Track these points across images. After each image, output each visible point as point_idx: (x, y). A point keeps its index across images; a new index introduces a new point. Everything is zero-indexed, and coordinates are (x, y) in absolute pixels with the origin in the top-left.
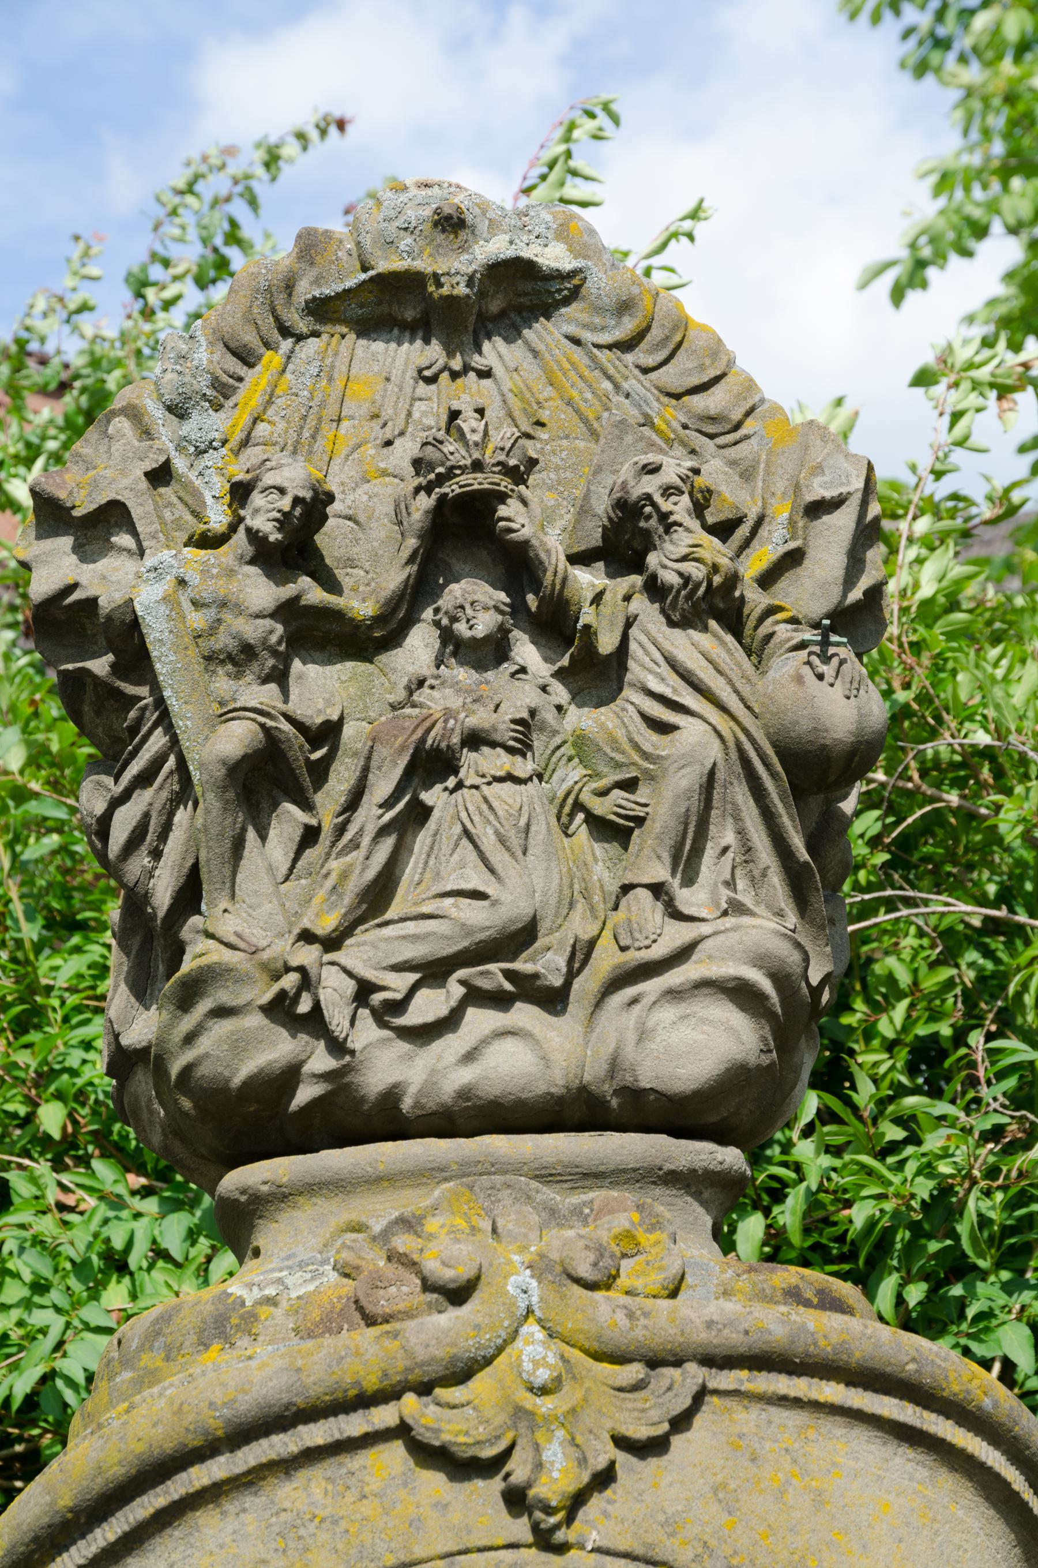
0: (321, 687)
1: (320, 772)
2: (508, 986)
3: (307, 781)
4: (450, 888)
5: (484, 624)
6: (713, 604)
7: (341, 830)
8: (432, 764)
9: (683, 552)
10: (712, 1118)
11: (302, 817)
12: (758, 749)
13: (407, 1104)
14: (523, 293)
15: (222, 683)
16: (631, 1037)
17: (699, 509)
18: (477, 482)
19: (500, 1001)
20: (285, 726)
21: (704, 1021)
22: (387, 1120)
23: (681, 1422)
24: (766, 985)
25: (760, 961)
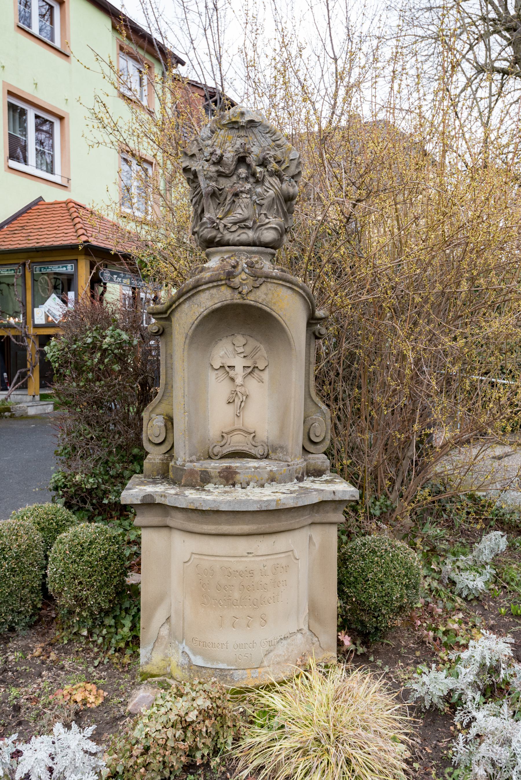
1: (221, 194)
4: (239, 213)
6: (277, 174)
8: (236, 195)
9: (273, 166)
15: (208, 181)
19: (243, 228)
22: (228, 244)
23: (261, 285)
24: (279, 228)
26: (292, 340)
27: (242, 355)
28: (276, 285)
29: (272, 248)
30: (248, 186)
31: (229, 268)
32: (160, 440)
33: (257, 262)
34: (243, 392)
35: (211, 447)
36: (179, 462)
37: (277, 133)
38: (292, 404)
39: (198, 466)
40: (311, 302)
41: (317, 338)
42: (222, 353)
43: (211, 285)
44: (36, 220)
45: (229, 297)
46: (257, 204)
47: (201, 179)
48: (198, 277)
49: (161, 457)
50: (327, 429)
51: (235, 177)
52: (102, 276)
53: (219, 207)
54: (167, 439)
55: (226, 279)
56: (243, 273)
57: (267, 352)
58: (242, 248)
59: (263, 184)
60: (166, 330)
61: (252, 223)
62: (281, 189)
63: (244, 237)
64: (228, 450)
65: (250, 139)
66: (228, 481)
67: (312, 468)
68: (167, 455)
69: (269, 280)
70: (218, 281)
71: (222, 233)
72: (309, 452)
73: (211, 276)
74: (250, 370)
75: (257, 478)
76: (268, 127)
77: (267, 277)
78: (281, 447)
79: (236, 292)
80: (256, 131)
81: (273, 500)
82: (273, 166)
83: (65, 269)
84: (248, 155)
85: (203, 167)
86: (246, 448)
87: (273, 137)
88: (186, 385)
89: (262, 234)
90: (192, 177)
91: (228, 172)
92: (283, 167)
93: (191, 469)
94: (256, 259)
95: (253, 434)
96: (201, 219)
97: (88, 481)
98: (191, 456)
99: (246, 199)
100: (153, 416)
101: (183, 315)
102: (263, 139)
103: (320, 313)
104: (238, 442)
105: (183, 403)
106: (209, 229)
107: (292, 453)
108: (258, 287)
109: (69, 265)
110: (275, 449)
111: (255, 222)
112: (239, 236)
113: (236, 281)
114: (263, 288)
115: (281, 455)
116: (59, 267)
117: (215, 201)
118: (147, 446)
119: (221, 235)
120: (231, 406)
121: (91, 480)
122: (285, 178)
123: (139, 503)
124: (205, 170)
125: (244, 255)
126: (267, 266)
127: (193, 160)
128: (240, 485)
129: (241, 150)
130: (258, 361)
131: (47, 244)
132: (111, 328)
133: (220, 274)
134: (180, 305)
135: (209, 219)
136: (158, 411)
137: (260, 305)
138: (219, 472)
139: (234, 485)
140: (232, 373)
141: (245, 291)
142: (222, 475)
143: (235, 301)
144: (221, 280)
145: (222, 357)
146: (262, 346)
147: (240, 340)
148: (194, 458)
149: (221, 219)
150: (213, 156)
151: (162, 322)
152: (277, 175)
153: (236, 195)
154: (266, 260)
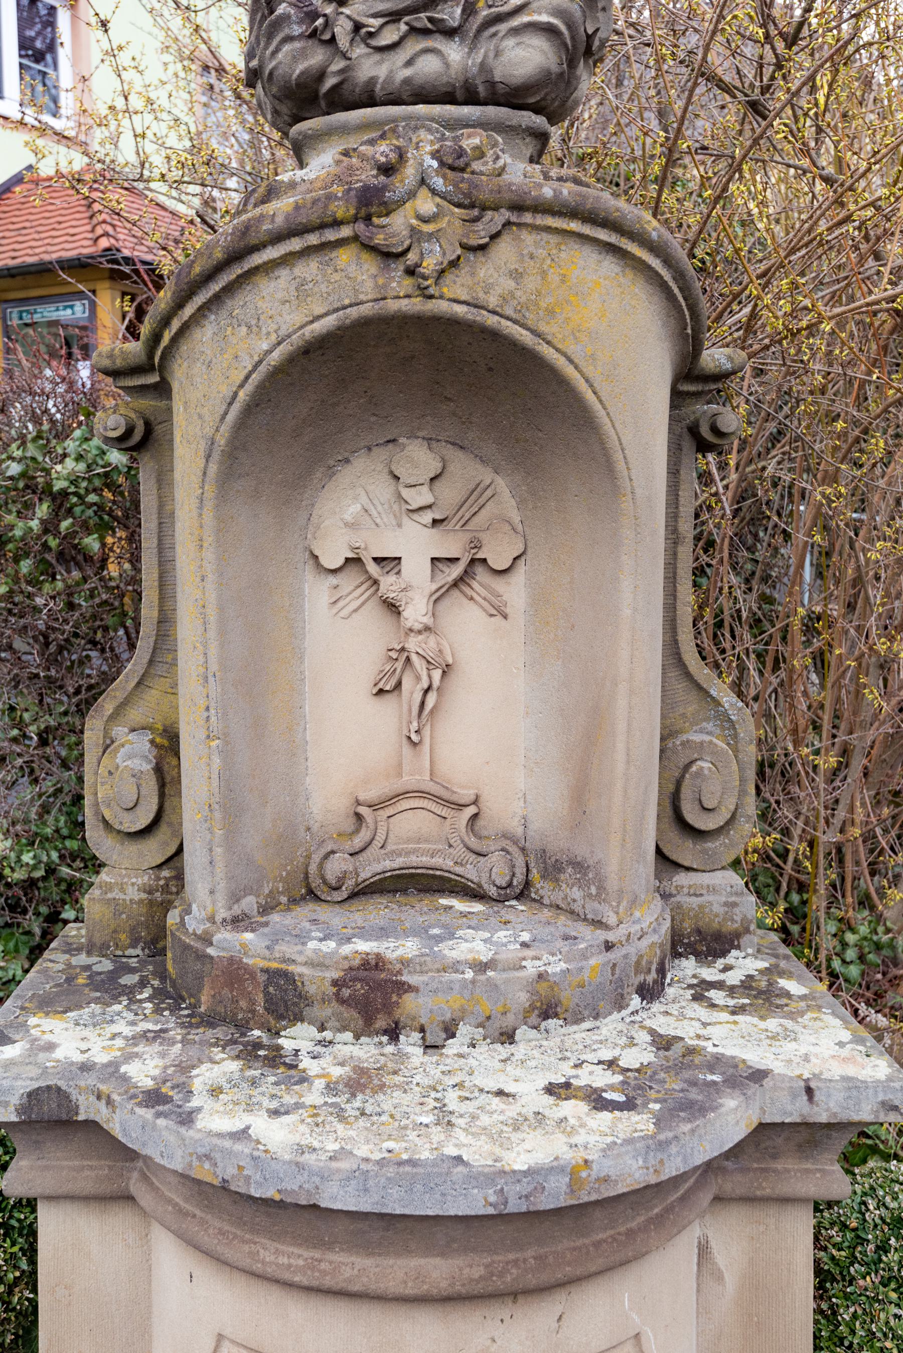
2: (429, 26)
10: (531, 100)
16: (491, 55)
19: (425, 32)
21: (529, 46)
23: (494, 237)
24: (563, 28)
25: (559, 12)
26: (619, 456)
28: (554, 239)
29: (537, 109)
31: (368, 176)
32: (143, 819)
33: (480, 153)
34: (430, 654)
35: (316, 858)
36: (195, 923)
38: (622, 703)
39: (252, 946)
41: (703, 447)
42: (352, 510)
43: (295, 244)
44: (17, 213)
45: (368, 290)
49: (144, 879)
50: (742, 780)
54: (165, 819)
55: (355, 219)
56: (424, 192)
57: (521, 504)
58: (421, 109)
60: (159, 429)
61: (459, 11)
63: (428, 67)
64: (378, 868)
66: (369, 1020)
67: (688, 926)
68: (166, 873)
69: (528, 218)
70: (322, 226)
71: (345, 56)
72: (678, 866)
73: (297, 207)
74: (456, 571)
75: (486, 1007)
77: (518, 207)
78: (579, 866)
79: (398, 269)
81: (555, 1169)
83: (69, 311)
86: (444, 862)
88: (212, 634)
89: (497, 54)
93: (231, 960)
94: (477, 141)
95: (472, 810)
97: (19, 860)
98: (235, 898)
100: (120, 731)
101: (199, 368)
103: (715, 357)
104: (414, 837)
105: (203, 703)
106: (297, 45)
107: (621, 891)
108: (482, 248)
109: (78, 303)
110: (553, 869)
112: (409, 63)
113: (397, 225)
114: (505, 252)
115: (576, 893)
116: (57, 310)
118: (97, 840)
120: (389, 701)
121: (27, 858)
123: (14, 1118)
125: (429, 130)
128: (416, 1036)
130: (485, 537)
131: (31, 260)
134: (185, 328)
136: (135, 715)
137: (492, 321)
138: (335, 983)
139: (393, 1034)
140: (389, 584)
141: (430, 265)
142: (346, 992)
143: (393, 306)
144: (337, 223)
145: (352, 526)
146: (501, 484)
147: (418, 458)
148: (249, 903)
151: (146, 403)
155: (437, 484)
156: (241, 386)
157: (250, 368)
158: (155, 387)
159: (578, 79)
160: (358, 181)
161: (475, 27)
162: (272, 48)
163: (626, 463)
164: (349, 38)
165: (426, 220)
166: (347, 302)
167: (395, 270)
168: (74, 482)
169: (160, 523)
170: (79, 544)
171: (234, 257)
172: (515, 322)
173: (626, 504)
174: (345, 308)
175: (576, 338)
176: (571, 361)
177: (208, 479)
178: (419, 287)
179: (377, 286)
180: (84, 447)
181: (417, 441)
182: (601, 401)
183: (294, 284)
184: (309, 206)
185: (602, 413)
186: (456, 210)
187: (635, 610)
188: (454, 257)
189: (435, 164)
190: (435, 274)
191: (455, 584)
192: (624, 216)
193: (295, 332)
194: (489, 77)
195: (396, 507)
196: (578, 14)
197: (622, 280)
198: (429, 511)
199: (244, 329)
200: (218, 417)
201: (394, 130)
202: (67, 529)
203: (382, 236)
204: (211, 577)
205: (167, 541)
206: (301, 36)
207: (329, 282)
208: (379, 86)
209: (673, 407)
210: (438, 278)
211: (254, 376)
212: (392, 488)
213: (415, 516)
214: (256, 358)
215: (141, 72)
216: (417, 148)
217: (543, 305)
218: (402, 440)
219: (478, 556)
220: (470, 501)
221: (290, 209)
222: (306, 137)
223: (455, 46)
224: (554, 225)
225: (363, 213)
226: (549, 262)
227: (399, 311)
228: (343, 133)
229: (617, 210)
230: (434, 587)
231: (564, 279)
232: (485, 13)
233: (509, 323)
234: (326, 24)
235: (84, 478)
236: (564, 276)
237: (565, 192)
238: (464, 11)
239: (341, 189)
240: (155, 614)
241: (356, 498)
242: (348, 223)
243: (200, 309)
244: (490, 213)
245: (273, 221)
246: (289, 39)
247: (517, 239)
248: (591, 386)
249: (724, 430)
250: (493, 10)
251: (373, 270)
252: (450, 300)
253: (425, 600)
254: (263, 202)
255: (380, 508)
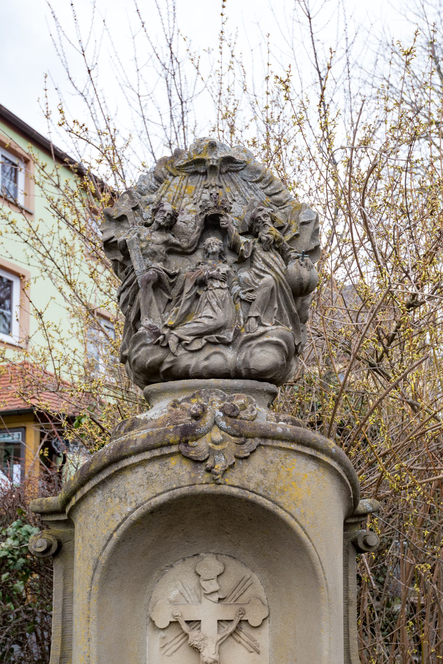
0: (177, 264)
1: (173, 285)
2: (217, 341)
3: (169, 287)
4: (209, 315)
5: (216, 248)
6: (275, 246)
7: (177, 300)
8: (201, 283)
9: (269, 232)
10: (269, 377)
11: (167, 297)
12: (286, 286)
13: (191, 370)
14: (230, 165)
15: (148, 261)
16: (248, 355)
17: (273, 222)
18: (216, 211)
19: (215, 344)
20: (164, 273)
21: (267, 352)
22: (186, 375)
23: (252, 452)
24: (284, 343)
25: (282, 336)
26: (319, 567)
27: (216, 597)
28: (283, 453)
29: (271, 381)
30: (224, 268)
31: (186, 420)
33: (244, 407)
37: (275, 182)
40: (353, 485)
42: (174, 594)
43: (147, 455)
45: (186, 480)
46: (242, 300)
47: (134, 255)
48: (123, 438)
51: (199, 256)
52: (56, 445)
53: (168, 307)
55: (180, 443)
56: (215, 428)
58: (213, 381)
59: (252, 265)
60: (66, 545)
61: (232, 334)
62: (286, 273)
65: (227, 190)
69: (269, 442)
70: (162, 446)
71: (173, 354)
73: (149, 436)
74: (231, 628)
76: (259, 172)
77: (264, 437)
79: (202, 469)
80: (237, 178)
82: (269, 232)
84: (223, 212)
85: (139, 235)
87: (269, 189)
89: (251, 355)
90: (120, 258)
91: (185, 245)
92: (288, 236)
94: (242, 401)
96: (136, 331)
99: (220, 291)
101: (91, 519)
102: (251, 192)
103: (365, 504)
106: (149, 348)
108: (246, 458)
111: (237, 333)
112: (207, 359)
113: (202, 445)
114: (258, 460)
116: (4, 437)
117: (162, 296)
119: (172, 358)
122: (293, 255)
124: (142, 241)
125: (217, 394)
126: (262, 415)
127: (123, 227)
129: (212, 204)
130: (247, 608)
132: (15, 524)
133: (166, 431)
135: (150, 328)
137: (252, 496)
140: (194, 636)
141: (219, 467)
143: (199, 488)
144: (170, 445)
145: (174, 603)
146: (255, 577)
147: (211, 565)
149: (172, 328)
150: (158, 214)
152: (277, 249)
153: (201, 283)
154: (260, 405)
155: (221, 578)
156: (115, 531)
157: (120, 521)
158: (64, 521)
159: (291, 366)
160: (181, 422)
161: (240, 342)
162: (135, 349)
163: (323, 570)
164: (176, 346)
165: (217, 444)
166: (174, 486)
167: (200, 469)
168: (11, 552)
169: (64, 599)
170: (12, 587)
171: (114, 461)
172: (264, 497)
173: (324, 593)
174: (173, 489)
175: (295, 505)
176: (293, 517)
177: (94, 583)
178: (213, 479)
179: (190, 477)
180: (18, 531)
181: (210, 555)
182: (309, 538)
183: (146, 476)
184: (155, 436)
185: (310, 544)
186: (233, 438)
187: (330, 652)
188: (231, 463)
189: (221, 414)
190: (222, 473)
191: (231, 635)
192: (318, 442)
193: (146, 502)
194: (247, 366)
195: (198, 591)
196: (291, 337)
197: (318, 473)
198: (216, 594)
199: (118, 500)
200: (101, 547)
201: (199, 393)
202: (6, 579)
203: (193, 452)
204: (94, 639)
205: (68, 610)
206: (151, 344)
207: (165, 475)
208: (191, 369)
209: (345, 530)
210: (223, 474)
211: (122, 525)
212: (196, 581)
213: (209, 597)
214: (124, 516)
215: (59, 333)
216: (212, 404)
217: (278, 487)
218: (202, 554)
219: (243, 619)
220: (239, 587)
221: (145, 437)
222: (152, 392)
223: (230, 351)
224: (283, 446)
225: (184, 439)
226: (280, 465)
227: (203, 491)
228: (172, 392)
229: (315, 439)
230: (219, 637)
231: (288, 473)
232: (245, 336)
233: (261, 498)
234: (164, 339)
235: (17, 549)
236: (289, 472)
237: (288, 430)
238: (234, 334)
239: (172, 427)
240: (59, 653)
241: (176, 587)
242: (176, 444)
243: (93, 488)
244: (250, 440)
245: (135, 443)
246: (145, 345)
247: (264, 453)
248: (304, 530)
249: (370, 544)
250: (249, 334)
251: (189, 469)
252: (229, 485)
253: (214, 645)
254: (130, 429)
255: (189, 592)
